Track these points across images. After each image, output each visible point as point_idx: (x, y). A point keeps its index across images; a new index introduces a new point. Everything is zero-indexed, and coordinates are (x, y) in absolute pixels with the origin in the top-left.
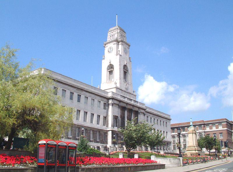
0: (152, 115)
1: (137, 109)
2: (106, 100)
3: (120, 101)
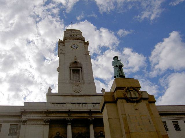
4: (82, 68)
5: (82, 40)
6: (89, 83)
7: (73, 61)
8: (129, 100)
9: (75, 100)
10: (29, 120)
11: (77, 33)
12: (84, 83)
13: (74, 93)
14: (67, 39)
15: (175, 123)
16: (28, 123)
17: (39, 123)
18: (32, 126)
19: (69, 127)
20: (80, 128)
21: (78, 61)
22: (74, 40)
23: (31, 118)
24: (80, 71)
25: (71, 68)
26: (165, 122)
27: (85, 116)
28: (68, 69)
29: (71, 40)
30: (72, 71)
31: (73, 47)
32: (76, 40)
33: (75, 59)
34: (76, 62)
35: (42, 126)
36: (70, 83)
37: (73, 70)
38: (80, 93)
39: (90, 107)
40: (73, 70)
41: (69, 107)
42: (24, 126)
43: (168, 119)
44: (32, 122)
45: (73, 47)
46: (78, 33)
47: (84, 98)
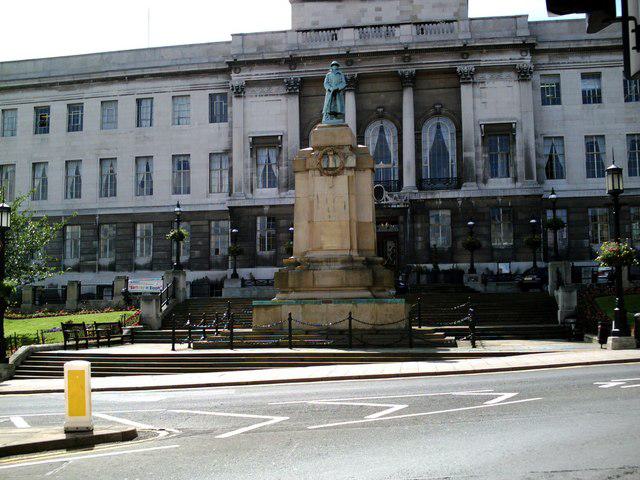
10: (249, 84)
17: (274, 89)
23: (254, 78)
35: (283, 98)
44: (257, 90)
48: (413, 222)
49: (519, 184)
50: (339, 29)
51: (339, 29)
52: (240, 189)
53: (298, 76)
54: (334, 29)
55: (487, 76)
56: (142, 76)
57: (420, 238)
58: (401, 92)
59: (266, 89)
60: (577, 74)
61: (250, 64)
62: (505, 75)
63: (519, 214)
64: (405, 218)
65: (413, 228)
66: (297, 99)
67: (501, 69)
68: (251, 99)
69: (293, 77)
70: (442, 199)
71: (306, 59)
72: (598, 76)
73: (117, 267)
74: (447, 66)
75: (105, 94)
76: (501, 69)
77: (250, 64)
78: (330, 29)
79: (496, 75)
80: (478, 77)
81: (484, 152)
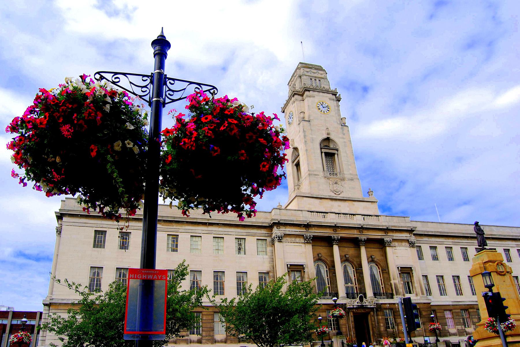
0: (449, 242)
1: (377, 235)
2: (263, 231)
3: (308, 226)
4: (337, 150)
5: (333, 94)
6: (352, 180)
7: (325, 136)
8: (500, 274)
9: (337, 207)
10: (286, 235)
11: (320, 76)
12: (343, 179)
13: (333, 195)
14: (309, 91)
15: (449, 250)
16: (284, 240)
17: (298, 240)
18: (290, 244)
19: (336, 248)
20: (346, 249)
21: (332, 137)
22: (321, 94)
23: (288, 233)
24: (336, 156)
25: (323, 150)
26: (508, 250)
27: (354, 234)
28: (319, 151)
29: (316, 93)
30: (323, 154)
31: (321, 107)
32: (323, 94)
33: (328, 134)
34: (328, 139)
35: (303, 245)
36: (325, 177)
37: (326, 153)
38: (340, 195)
39: (358, 221)
40: (326, 153)
41: (331, 219)
42: (280, 243)
43: (456, 244)
44: (289, 239)
45: (321, 107)
46: (321, 74)
47: (347, 203)
48: (377, 315)
49: (419, 297)
50: (327, 213)
51: (327, 213)
52: (335, 192)
53: (312, 234)
54: (325, 213)
55: (396, 244)
56: (218, 224)
57: (382, 325)
58: (332, 246)
59: (293, 239)
60: (427, 246)
61: (286, 225)
62: (404, 244)
63: (423, 312)
64: (374, 313)
65: (377, 319)
66: (139, 268)
67: (402, 241)
68: (287, 244)
69: (308, 234)
70: (389, 304)
71: (314, 226)
72: (435, 248)
73: (203, 341)
74: (379, 237)
75: (193, 231)
76: (402, 241)
77: (286, 225)
78: (323, 213)
79: (400, 244)
80: (393, 244)
81: (401, 281)
